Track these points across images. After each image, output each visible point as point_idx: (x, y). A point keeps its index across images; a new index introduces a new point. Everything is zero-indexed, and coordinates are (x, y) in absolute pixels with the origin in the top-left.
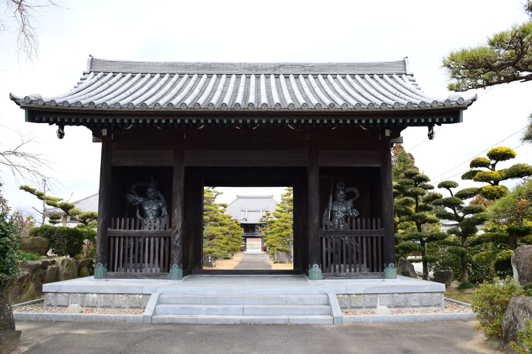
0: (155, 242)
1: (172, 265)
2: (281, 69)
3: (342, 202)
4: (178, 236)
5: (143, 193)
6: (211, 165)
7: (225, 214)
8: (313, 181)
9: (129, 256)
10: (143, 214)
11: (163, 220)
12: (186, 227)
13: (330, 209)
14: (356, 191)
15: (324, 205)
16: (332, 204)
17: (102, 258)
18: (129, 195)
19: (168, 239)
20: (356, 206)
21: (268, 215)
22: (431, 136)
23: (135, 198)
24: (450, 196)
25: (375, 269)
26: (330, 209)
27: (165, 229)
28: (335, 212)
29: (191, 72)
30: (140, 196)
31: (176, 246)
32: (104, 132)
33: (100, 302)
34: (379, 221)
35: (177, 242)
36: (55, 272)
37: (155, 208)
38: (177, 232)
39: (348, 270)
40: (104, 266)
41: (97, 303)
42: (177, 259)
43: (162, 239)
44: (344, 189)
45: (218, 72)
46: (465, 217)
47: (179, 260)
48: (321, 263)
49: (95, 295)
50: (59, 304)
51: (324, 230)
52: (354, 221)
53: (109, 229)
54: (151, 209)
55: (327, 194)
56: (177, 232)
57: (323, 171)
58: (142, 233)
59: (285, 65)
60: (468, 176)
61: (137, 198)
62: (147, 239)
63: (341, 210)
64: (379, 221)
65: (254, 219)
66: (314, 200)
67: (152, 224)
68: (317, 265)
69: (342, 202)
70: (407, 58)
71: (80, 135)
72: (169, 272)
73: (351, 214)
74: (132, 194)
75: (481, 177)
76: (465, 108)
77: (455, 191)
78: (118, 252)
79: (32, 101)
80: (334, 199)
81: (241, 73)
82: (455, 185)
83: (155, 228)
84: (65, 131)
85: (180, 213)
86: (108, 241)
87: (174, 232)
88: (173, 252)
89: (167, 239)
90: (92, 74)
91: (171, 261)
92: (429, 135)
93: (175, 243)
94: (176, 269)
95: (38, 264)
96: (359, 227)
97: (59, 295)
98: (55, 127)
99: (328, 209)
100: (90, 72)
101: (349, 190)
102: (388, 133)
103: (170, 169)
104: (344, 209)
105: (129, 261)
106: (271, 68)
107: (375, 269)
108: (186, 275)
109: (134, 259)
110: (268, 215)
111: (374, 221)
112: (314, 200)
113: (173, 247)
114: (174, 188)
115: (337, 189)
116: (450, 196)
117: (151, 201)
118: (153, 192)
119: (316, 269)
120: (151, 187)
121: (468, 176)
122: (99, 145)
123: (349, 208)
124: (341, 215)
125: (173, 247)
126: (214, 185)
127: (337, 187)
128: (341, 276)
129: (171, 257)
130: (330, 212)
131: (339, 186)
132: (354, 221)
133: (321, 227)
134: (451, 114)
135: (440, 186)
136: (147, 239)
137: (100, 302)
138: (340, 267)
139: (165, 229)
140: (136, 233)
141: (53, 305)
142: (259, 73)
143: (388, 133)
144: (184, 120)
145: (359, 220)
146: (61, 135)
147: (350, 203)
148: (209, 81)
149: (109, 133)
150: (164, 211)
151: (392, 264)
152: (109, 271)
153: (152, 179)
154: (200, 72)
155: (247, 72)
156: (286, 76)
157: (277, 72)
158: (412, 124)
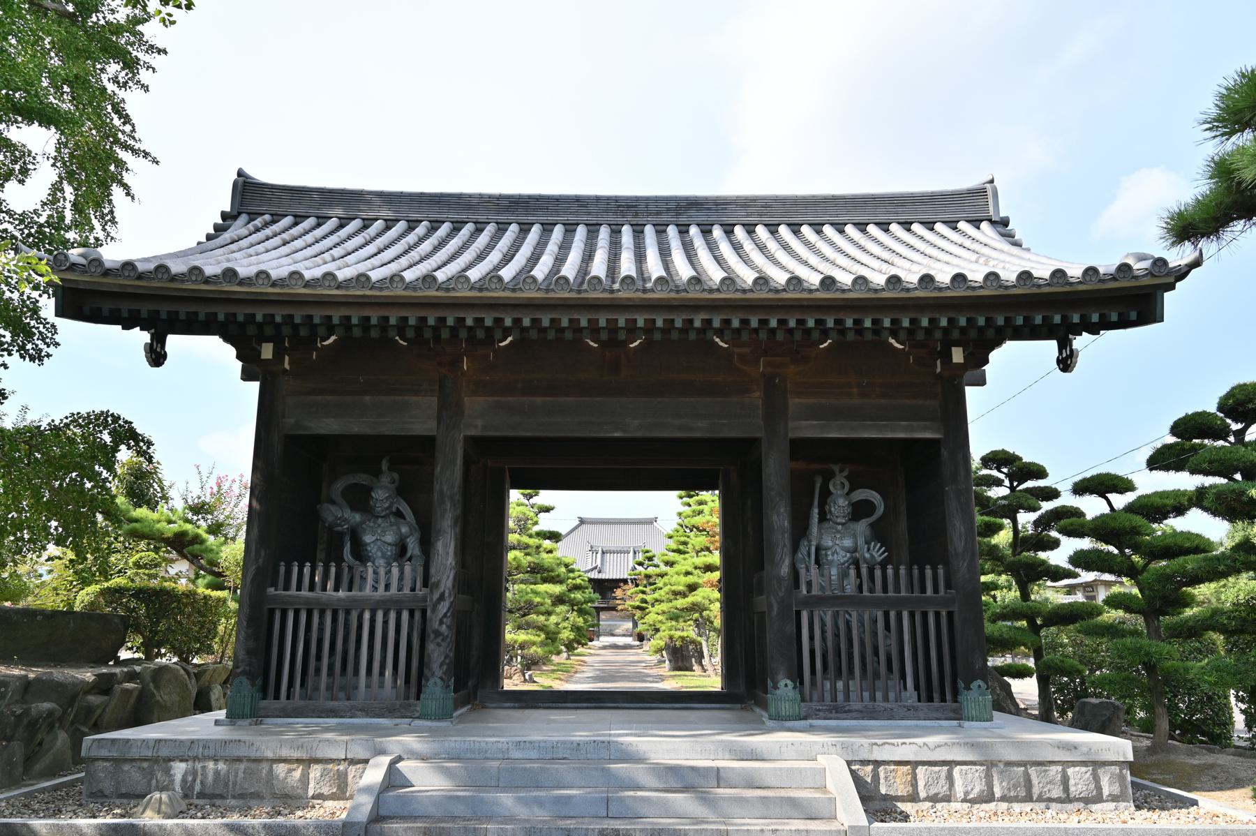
0: (386, 623)
1: (427, 680)
2: (693, 212)
3: (843, 524)
4: (443, 608)
5: (360, 499)
6: (529, 434)
7: (557, 554)
8: (775, 470)
9: (319, 657)
10: (360, 554)
11: (408, 568)
12: (464, 583)
13: (814, 543)
14: (875, 497)
15: (800, 531)
16: (820, 531)
17: (249, 664)
18: (326, 506)
19: (420, 614)
20: (879, 533)
21: (650, 559)
22: (1066, 363)
23: (339, 514)
24: (1107, 510)
25: (936, 696)
26: (814, 543)
27: (413, 589)
28: (827, 549)
29: (482, 218)
30: (354, 508)
31: (438, 633)
32: (267, 351)
33: (235, 784)
34: (941, 572)
35: (441, 622)
36: (132, 701)
37: (389, 538)
38: (442, 598)
39: (866, 695)
40: (253, 685)
41: (226, 784)
42: (441, 665)
43: (405, 615)
44: (848, 494)
45: (543, 219)
46: (1152, 565)
47: (445, 667)
48: (798, 677)
49: (221, 766)
50: (123, 791)
51: (805, 592)
52: (878, 573)
53: (271, 590)
54: (379, 538)
55: (806, 502)
56: (442, 598)
57: (800, 448)
58: (354, 600)
59: (702, 204)
60: (1161, 460)
61: (348, 514)
62: (367, 615)
63: (841, 543)
64: (941, 572)
65: (615, 569)
66: (779, 518)
67: (383, 579)
68: (789, 682)
69: (843, 524)
70: (992, 181)
71: (206, 358)
72: (418, 699)
73: (867, 555)
74: (333, 502)
75: (1211, 462)
76: (1171, 287)
77: (1120, 501)
78: (290, 649)
79: (74, 264)
80: (823, 518)
81: (600, 220)
82: (1123, 485)
83: (387, 587)
84: (167, 349)
85: (451, 550)
86: (260, 619)
87: (436, 596)
88: (431, 647)
89: (417, 615)
90: (244, 218)
91: (426, 671)
92: (1059, 362)
93: (436, 625)
94: (436, 688)
95: (83, 682)
96: (891, 587)
97: (126, 767)
98: (140, 337)
99: (809, 541)
100: (240, 214)
101: (861, 494)
102: (958, 355)
103: (427, 444)
104: (848, 543)
105: (318, 671)
106: (668, 210)
107: (936, 696)
108: (463, 705)
109: (331, 667)
110: (650, 559)
111: (929, 572)
112: (779, 518)
113: (432, 636)
114: (437, 487)
115: (830, 493)
116: (1107, 510)
117: (380, 520)
118: (387, 498)
119: (785, 688)
120: (381, 488)
121: (1161, 460)
122: (255, 386)
123: (861, 541)
124: (842, 557)
125: (432, 636)
126: (534, 482)
127: (831, 488)
128: (850, 711)
129: (426, 659)
130: (813, 549)
131: (834, 485)
132: (878, 573)
133: (797, 585)
134: (1129, 300)
135: (1081, 488)
136: (367, 615)
137: (235, 784)
138: (847, 687)
139: (413, 589)
140: (340, 600)
141: (107, 792)
142: (640, 220)
143: (958, 355)
144: (463, 319)
145: (890, 570)
146: (156, 356)
147: (862, 527)
148: (524, 238)
149: (278, 354)
150: (413, 547)
151: (979, 682)
152: (264, 698)
153: (385, 465)
154: (503, 218)
155: (612, 219)
156: (705, 228)
157: (683, 220)
158: (1018, 335)
